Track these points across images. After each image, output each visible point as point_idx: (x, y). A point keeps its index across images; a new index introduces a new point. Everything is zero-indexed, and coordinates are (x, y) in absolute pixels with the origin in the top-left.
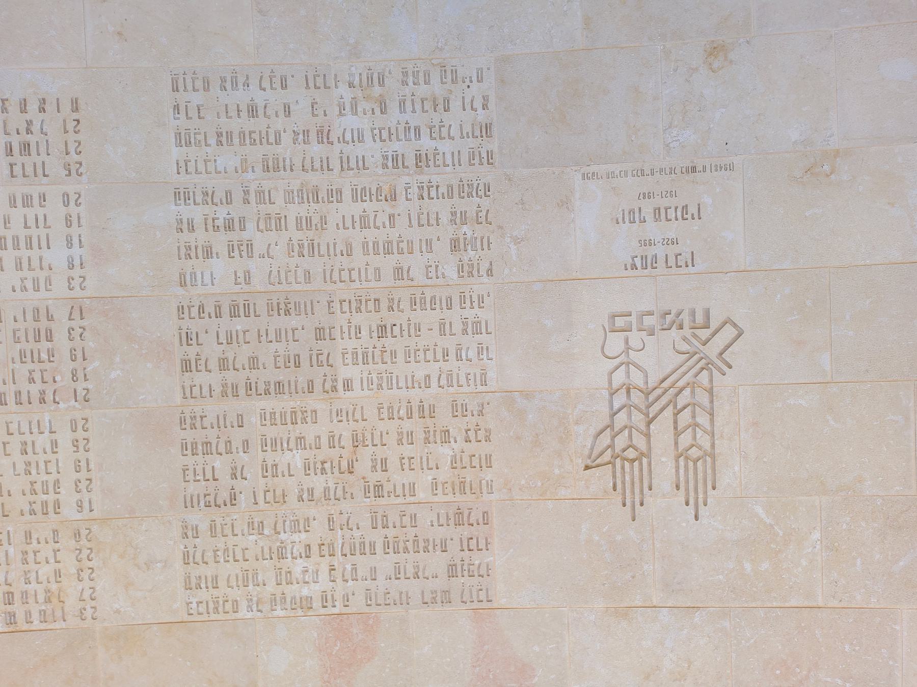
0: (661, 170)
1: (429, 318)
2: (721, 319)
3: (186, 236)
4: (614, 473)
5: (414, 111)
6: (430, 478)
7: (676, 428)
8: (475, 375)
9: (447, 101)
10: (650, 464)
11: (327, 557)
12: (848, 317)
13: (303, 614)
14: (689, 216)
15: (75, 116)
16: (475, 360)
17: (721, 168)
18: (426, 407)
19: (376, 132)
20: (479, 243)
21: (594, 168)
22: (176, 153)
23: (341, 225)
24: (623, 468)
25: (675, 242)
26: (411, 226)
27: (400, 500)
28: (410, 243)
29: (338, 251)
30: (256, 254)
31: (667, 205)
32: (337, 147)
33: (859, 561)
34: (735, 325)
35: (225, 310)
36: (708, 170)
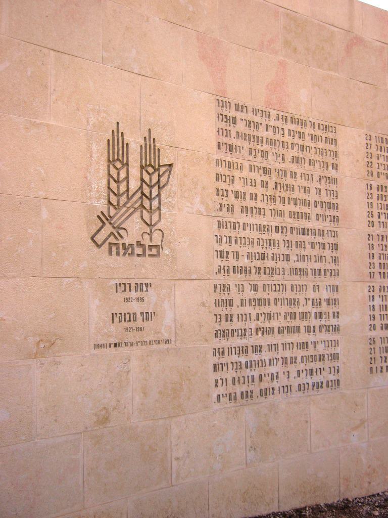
0: (132, 345)
1: (244, 262)
2: (102, 248)
3: (336, 310)
4: (159, 160)
5: (248, 377)
6: (243, 173)
7: (128, 182)
8: (223, 227)
9: (234, 383)
10: (141, 162)
11: (285, 142)
12: (31, 242)
13: (295, 116)
14: (119, 315)
15: (371, 365)
16: (223, 236)
17: (101, 346)
18: (245, 212)
19: (264, 365)
20: (220, 303)
21: (166, 346)
22: (338, 350)
23: (279, 314)
24: (154, 162)
25: (126, 300)
26: (250, 314)
27: (256, 164)
28: (250, 305)
29: (280, 301)
30: (311, 300)
31: (130, 323)
32: (279, 356)
33: (29, 73)
34: (95, 242)
35: (323, 273)
36: (108, 345)
